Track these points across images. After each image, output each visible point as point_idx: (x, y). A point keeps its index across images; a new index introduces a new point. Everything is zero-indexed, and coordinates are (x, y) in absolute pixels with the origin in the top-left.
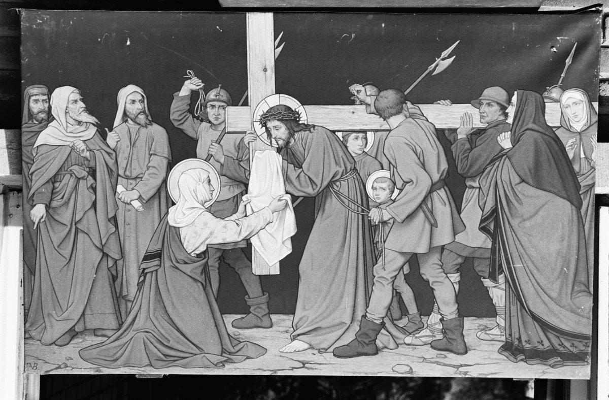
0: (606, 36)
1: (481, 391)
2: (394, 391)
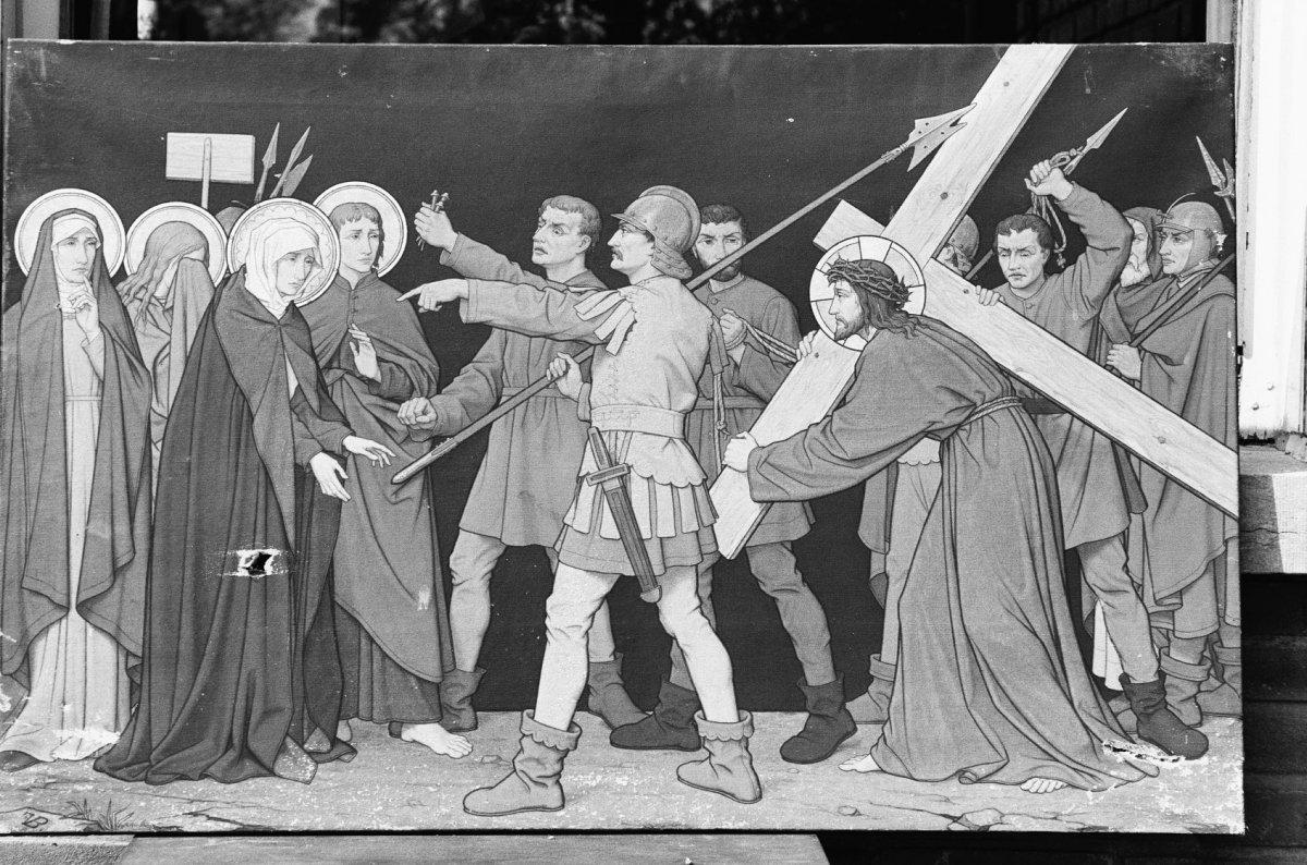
1: (252, 12)
2: (440, 13)
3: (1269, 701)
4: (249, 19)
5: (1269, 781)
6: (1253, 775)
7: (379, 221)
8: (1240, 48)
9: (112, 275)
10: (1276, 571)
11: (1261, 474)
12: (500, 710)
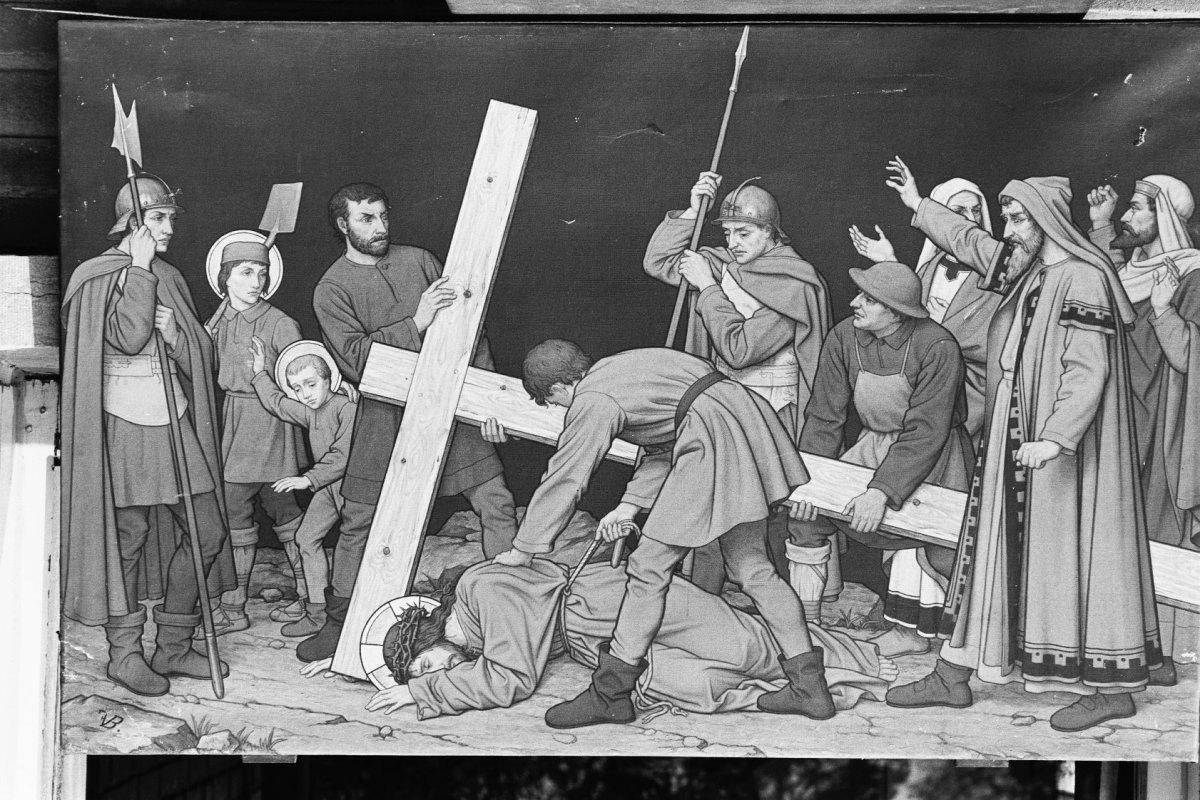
8: (55, 741)
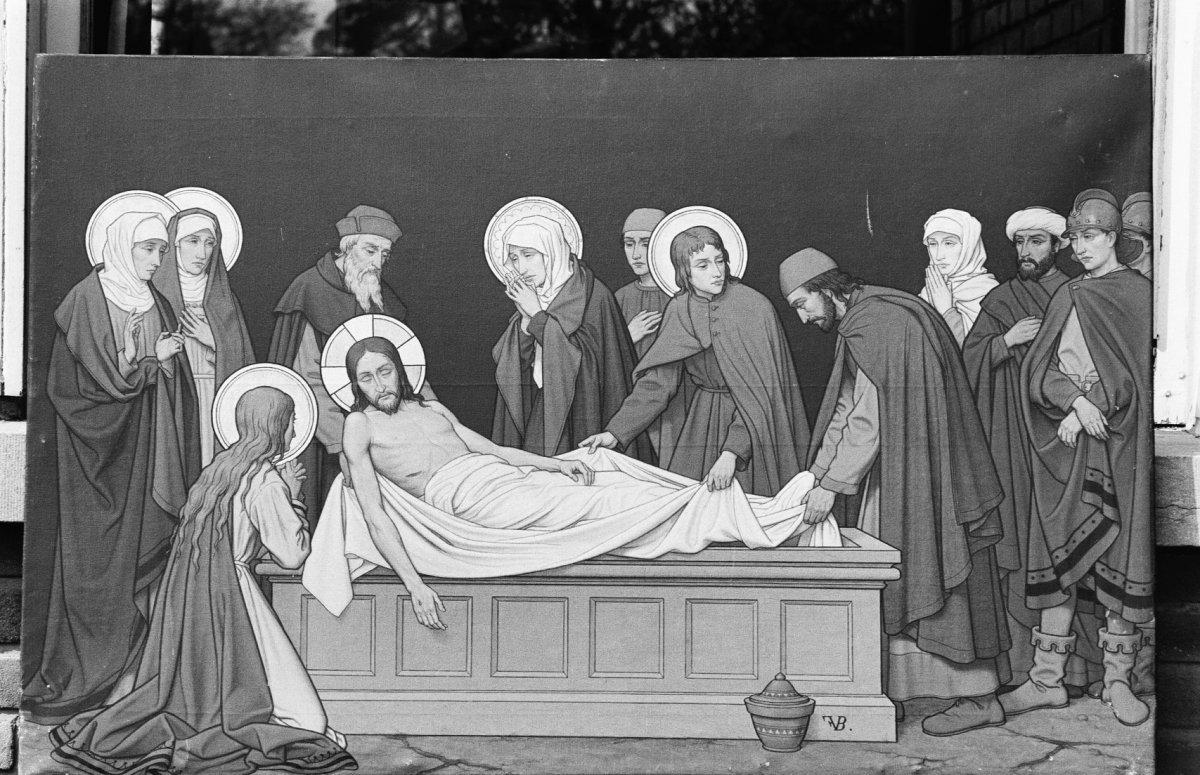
0: (10, 730)
1: (256, 32)
2: (426, 33)
3: (1179, 663)
4: (252, 39)
5: (1179, 735)
6: (1164, 730)
7: (719, 244)
9: (228, 269)
10: (1186, 543)
11: (1173, 455)
12: (879, 285)
